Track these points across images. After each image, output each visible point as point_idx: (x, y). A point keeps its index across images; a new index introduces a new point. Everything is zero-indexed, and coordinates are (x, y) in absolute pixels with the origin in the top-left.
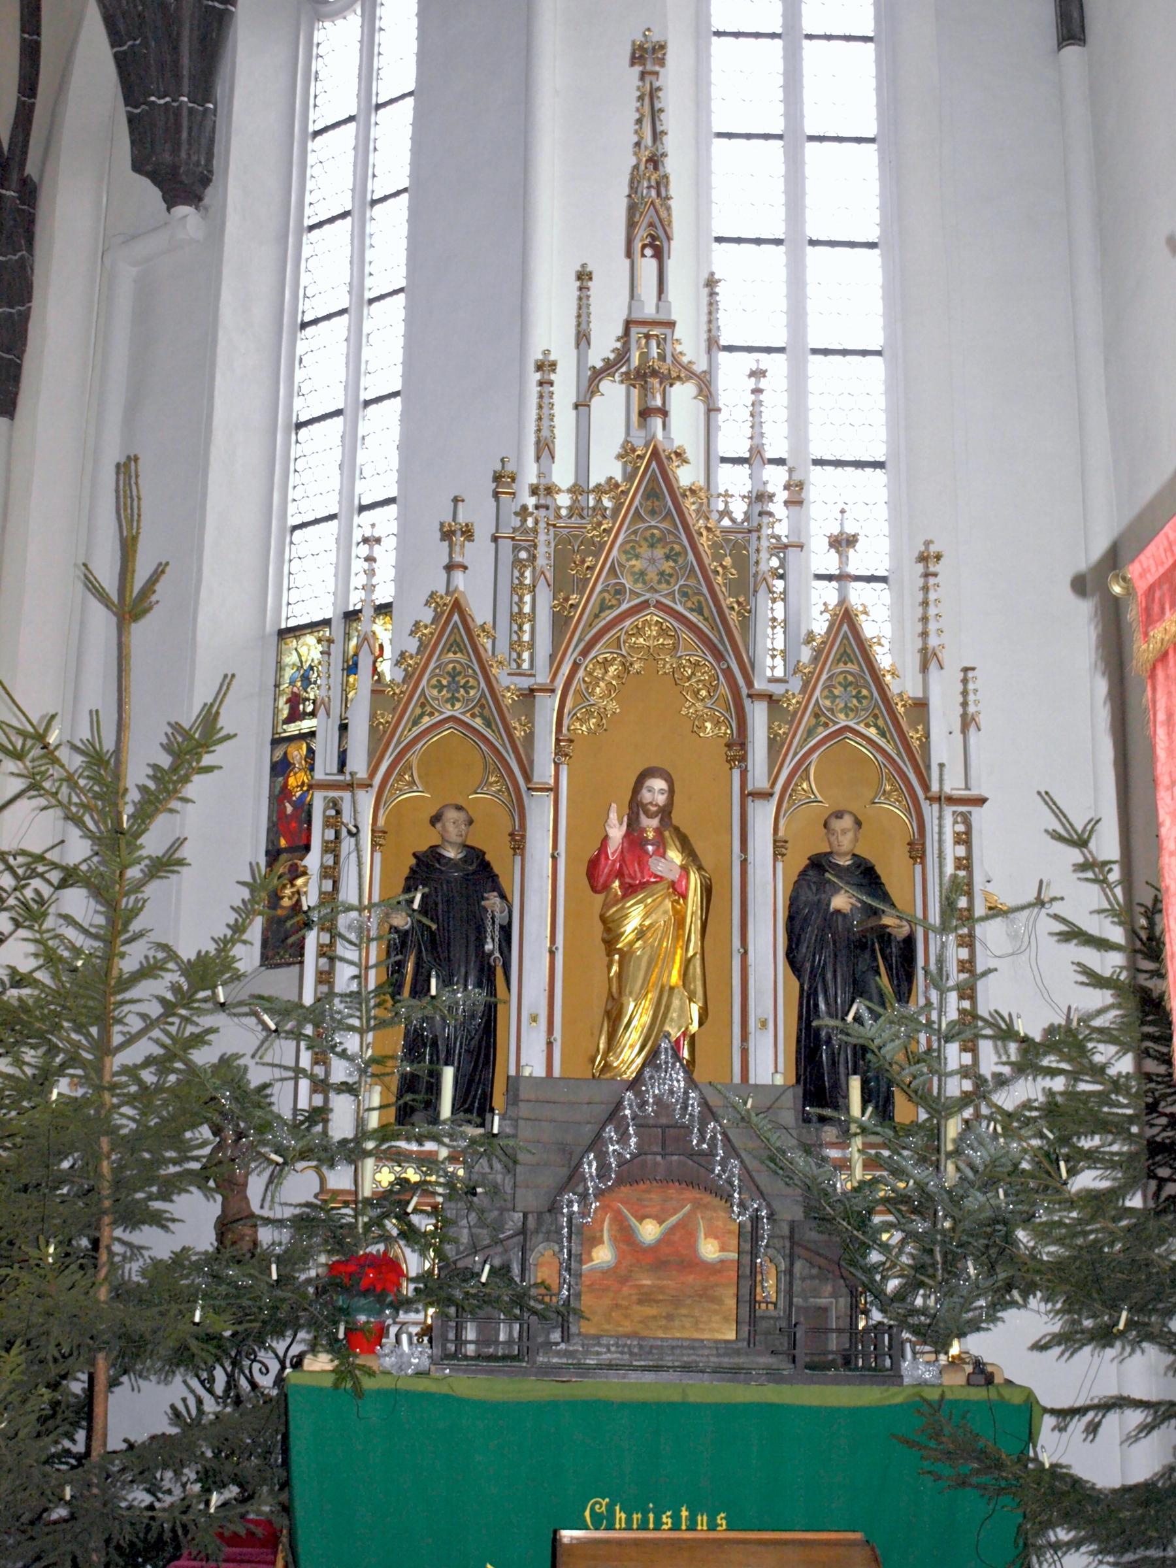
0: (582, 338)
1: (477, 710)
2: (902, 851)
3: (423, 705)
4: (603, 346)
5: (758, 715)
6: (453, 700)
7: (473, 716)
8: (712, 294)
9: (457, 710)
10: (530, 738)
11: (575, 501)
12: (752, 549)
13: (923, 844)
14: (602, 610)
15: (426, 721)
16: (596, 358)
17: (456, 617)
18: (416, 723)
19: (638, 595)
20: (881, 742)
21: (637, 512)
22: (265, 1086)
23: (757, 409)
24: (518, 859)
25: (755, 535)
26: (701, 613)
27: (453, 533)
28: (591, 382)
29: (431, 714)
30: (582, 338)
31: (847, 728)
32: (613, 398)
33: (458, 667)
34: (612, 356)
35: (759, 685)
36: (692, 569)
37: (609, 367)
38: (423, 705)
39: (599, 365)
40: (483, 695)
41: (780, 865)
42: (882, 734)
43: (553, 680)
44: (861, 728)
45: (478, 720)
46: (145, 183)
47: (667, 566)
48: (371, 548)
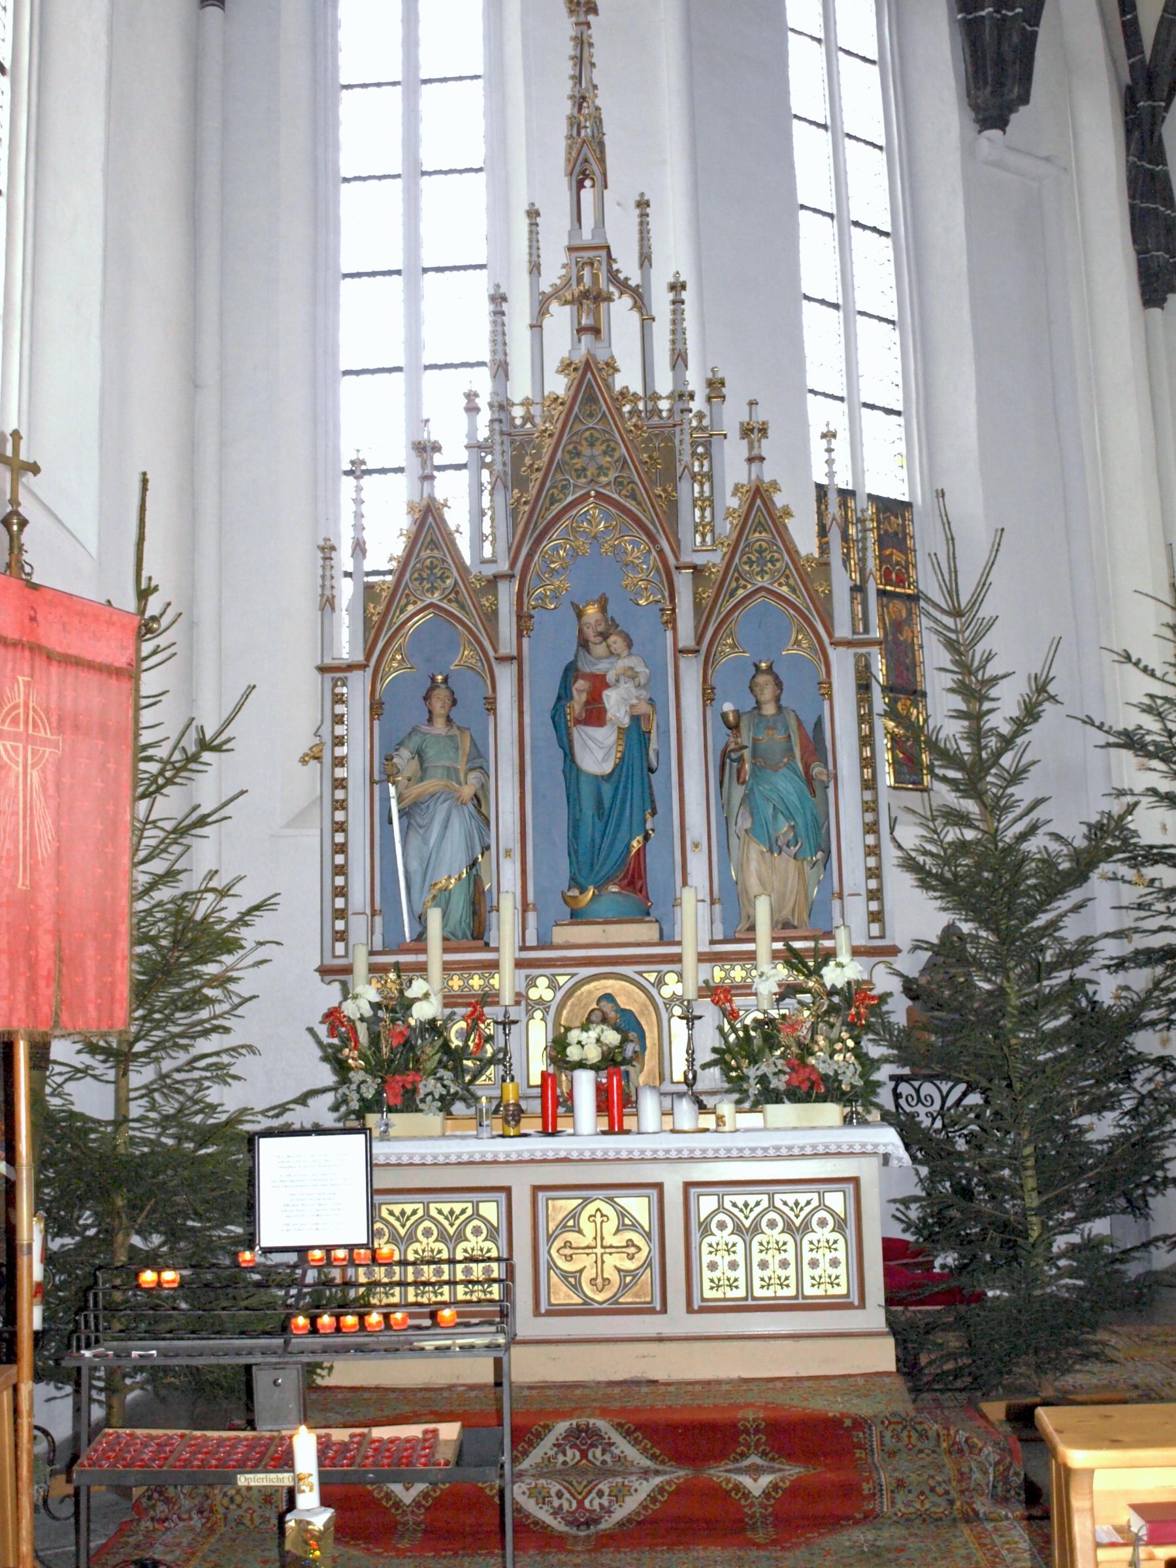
0: (535, 268)
1: (452, 596)
2: (480, 705)
3: (737, 580)
4: (551, 276)
5: (684, 582)
6: (762, 573)
7: (780, 585)
8: (644, 215)
9: (435, 598)
10: (829, 597)
11: (528, 411)
12: (677, 442)
13: (830, 684)
14: (552, 504)
15: (741, 593)
16: (545, 286)
17: (758, 502)
18: (732, 594)
19: (581, 488)
20: (792, 597)
21: (577, 417)
22: (926, 879)
23: (679, 317)
24: (491, 718)
25: (678, 429)
26: (635, 499)
27: (752, 430)
28: (541, 308)
29: (415, 603)
30: (535, 268)
31: (762, 589)
32: (561, 318)
33: (764, 545)
34: (558, 282)
35: (686, 558)
36: (625, 462)
37: (556, 293)
38: (737, 580)
39: (548, 290)
40: (456, 583)
41: (376, 723)
42: (793, 590)
43: (513, 565)
44: (775, 587)
45: (785, 588)
46: (1014, 118)
47: (578, 463)
48: (829, 442)
